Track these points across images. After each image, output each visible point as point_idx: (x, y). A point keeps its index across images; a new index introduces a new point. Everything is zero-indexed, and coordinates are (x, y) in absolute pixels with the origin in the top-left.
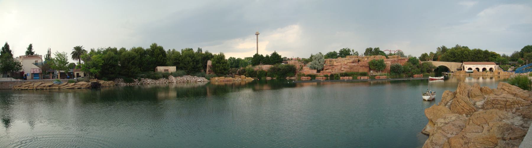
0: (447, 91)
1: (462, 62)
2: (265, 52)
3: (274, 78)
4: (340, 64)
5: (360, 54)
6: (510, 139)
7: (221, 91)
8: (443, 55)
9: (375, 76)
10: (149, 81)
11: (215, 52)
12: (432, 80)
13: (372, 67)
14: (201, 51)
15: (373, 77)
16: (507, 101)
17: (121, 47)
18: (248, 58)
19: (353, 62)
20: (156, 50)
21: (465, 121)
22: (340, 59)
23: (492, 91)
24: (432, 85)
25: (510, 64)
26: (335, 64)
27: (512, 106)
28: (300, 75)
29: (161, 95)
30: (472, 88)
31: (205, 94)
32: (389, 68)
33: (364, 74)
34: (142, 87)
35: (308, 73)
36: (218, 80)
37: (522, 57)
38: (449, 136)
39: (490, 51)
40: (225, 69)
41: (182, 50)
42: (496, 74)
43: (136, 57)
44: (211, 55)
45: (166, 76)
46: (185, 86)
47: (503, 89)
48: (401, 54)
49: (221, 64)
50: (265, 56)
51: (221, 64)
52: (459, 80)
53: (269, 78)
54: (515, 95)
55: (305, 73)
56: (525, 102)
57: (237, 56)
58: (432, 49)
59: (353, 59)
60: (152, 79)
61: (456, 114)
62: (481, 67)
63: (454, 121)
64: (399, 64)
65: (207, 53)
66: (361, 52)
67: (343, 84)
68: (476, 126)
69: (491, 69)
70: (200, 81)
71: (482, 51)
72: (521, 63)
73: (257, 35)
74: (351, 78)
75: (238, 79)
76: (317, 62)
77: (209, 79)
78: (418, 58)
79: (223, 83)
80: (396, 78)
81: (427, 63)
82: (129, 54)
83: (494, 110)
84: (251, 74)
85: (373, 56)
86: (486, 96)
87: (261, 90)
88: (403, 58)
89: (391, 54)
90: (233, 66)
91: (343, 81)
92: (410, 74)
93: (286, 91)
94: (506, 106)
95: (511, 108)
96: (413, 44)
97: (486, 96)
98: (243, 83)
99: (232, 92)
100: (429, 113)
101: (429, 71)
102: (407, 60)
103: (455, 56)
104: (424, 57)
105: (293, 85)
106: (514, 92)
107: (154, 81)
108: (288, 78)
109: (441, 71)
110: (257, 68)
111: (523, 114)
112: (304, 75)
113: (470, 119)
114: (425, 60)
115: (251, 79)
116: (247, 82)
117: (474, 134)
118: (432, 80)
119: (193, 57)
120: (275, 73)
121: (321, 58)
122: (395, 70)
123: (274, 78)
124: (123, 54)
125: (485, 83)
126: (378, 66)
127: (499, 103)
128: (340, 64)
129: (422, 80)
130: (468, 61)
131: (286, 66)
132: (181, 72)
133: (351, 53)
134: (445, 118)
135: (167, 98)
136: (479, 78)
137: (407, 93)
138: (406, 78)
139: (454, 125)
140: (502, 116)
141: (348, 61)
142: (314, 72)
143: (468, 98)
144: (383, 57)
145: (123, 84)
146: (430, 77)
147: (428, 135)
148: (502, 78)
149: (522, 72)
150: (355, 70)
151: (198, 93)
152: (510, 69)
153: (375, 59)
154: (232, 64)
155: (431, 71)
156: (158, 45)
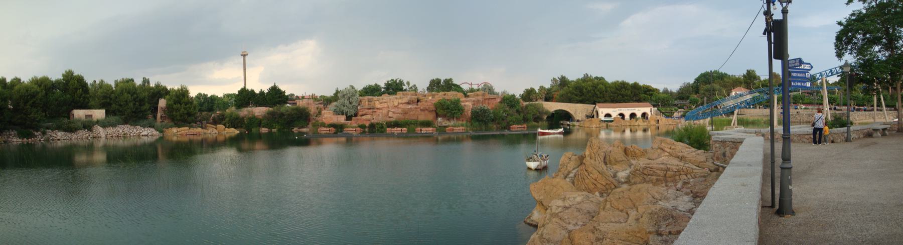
0: (569, 154)
1: (594, 103)
2: (258, 85)
3: (274, 130)
4: (385, 105)
5: (420, 90)
6: (670, 233)
7: (183, 153)
8: (561, 92)
9: (446, 127)
10: (60, 134)
11: (172, 84)
12: (543, 134)
13: (440, 112)
14: (149, 83)
15: (442, 130)
16: (668, 170)
17: (13, 77)
18: (228, 96)
19: (408, 103)
20: (72, 82)
21: (599, 203)
22: (386, 97)
23: (644, 153)
24: (542, 143)
25: (676, 105)
26: (378, 105)
27: (677, 177)
28: (318, 125)
29: (81, 158)
30: (610, 149)
31: (155, 157)
32: (470, 113)
33: (427, 124)
34: (49, 146)
35: (331, 122)
36: (177, 133)
37: (697, 92)
38: (571, 227)
39: (641, 84)
40: (189, 114)
41: (116, 81)
42: (653, 123)
43: (38, 93)
44: (165, 89)
45: (88, 125)
46: (121, 143)
47: (662, 149)
48: (488, 89)
49: (183, 105)
50: (257, 91)
51: (183, 105)
52: (589, 135)
53: (264, 130)
54: (682, 158)
55: (324, 121)
56: (698, 171)
57: (210, 92)
58: (543, 80)
59: (409, 97)
60: (65, 130)
61: (584, 193)
62: (627, 112)
63: (579, 203)
64: (486, 106)
65: (158, 86)
66: (422, 86)
67: (392, 141)
68: (617, 212)
69: (644, 115)
70: (146, 134)
71: (628, 84)
72: (694, 102)
73: (244, 56)
74: (405, 130)
75: (212, 132)
76: (347, 102)
77: (161, 132)
78: (518, 96)
79: (186, 139)
80: (481, 130)
81: (534, 106)
82: (27, 88)
83: (645, 185)
84: (235, 122)
85: (441, 93)
86: (633, 162)
87: (251, 150)
88: (492, 96)
89: (472, 90)
90: (204, 108)
91: (392, 135)
92: (504, 124)
93: (292, 153)
94: (666, 177)
95: (675, 181)
96: (510, 73)
97: (633, 162)
98: (221, 138)
99: (201, 153)
100: (537, 190)
101: (537, 119)
102: (499, 100)
103: (582, 93)
104: (529, 94)
105: (304, 142)
106: (680, 154)
107: (69, 135)
108: (295, 130)
109: (558, 119)
110: (244, 112)
111: (695, 191)
112: (323, 125)
113: (606, 201)
114: (531, 100)
115: (234, 132)
116: (227, 136)
117: (611, 224)
118: (543, 134)
119: (134, 93)
120: (275, 121)
121: (353, 95)
122: (480, 118)
123: (274, 130)
124: (16, 88)
125: (634, 140)
126: (450, 110)
127: (654, 174)
128: (385, 105)
129: (525, 135)
130: (605, 102)
131: (293, 109)
132: (113, 119)
133: (404, 88)
134: (564, 199)
135: (89, 164)
136: (624, 131)
137: (500, 156)
138: (497, 129)
139: (579, 210)
140: (657, 196)
141: (400, 101)
142: (342, 119)
143: (603, 166)
144: (460, 95)
145: (16, 141)
146: (539, 130)
147: (536, 226)
148: (663, 129)
149: (697, 119)
150: (411, 117)
151: (142, 156)
152: (676, 114)
153: (446, 97)
154: (201, 105)
155: (541, 119)
156: (76, 74)
